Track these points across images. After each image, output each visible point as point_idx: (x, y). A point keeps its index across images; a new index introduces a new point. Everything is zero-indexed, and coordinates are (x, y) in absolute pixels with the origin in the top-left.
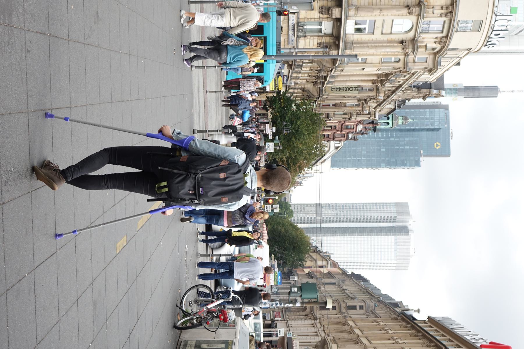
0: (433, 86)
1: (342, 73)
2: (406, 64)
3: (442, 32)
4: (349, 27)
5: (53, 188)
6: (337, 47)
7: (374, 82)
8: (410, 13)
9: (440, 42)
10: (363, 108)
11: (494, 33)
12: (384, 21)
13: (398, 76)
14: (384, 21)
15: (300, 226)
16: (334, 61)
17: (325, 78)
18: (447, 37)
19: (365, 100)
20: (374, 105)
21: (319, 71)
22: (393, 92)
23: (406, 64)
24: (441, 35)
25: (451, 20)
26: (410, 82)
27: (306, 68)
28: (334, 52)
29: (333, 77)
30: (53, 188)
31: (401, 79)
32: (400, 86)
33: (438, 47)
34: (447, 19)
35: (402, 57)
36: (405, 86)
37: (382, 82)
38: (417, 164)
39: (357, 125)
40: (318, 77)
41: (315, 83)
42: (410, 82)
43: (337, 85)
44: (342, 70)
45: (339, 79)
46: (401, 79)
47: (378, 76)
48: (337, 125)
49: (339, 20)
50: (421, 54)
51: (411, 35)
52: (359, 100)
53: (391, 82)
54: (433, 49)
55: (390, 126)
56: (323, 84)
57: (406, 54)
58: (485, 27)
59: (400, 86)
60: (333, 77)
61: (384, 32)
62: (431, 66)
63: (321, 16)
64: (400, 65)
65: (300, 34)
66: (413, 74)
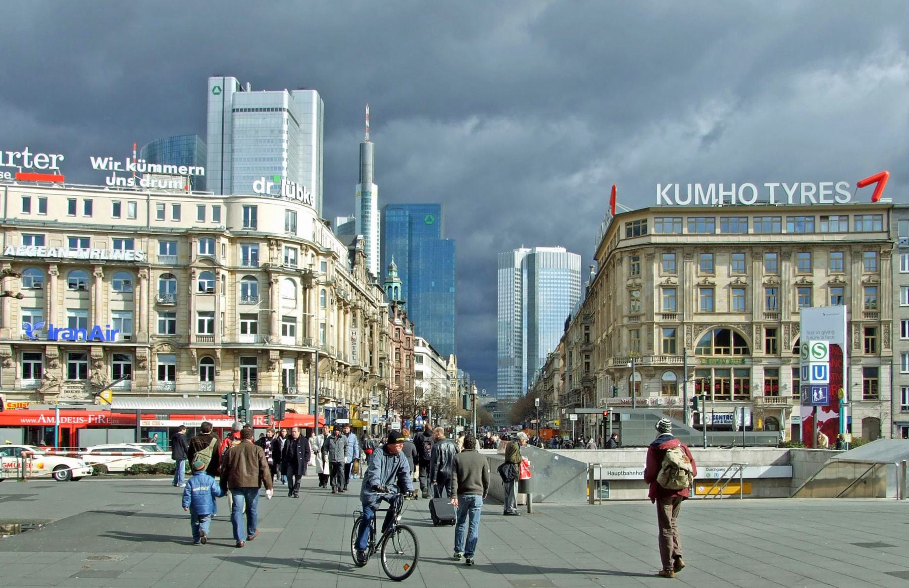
0: (352, 247)
1: (336, 347)
2: (328, 284)
3: (295, 249)
4: (289, 342)
5: (724, 288)
7: (346, 312)
8: (277, 281)
9: (306, 250)
10: (374, 321)
11: (298, 197)
12: (284, 307)
13: (340, 289)
14: (284, 307)
17: (340, 364)
18: (301, 244)
19: (366, 319)
20: (372, 308)
21: (333, 370)
22: (357, 290)
23: (328, 284)
24: (299, 251)
25: (285, 241)
26: (346, 274)
27: (330, 384)
28: (314, 356)
29: (339, 356)
30: (724, 288)
31: (343, 284)
32: (351, 284)
33: (311, 252)
34: (284, 245)
35: (321, 287)
36: (351, 278)
37: (345, 305)
39: (395, 325)
40: (339, 372)
41: (346, 374)
42: (346, 274)
43: (349, 352)
44: (332, 347)
45: (342, 349)
46: (343, 284)
47: (340, 308)
48: (394, 347)
49: (282, 352)
50: (317, 269)
52: (366, 326)
53: (346, 295)
54: (313, 256)
55: (399, 285)
56: (346, 366)
57: (317, 284)
58: (293, 206)
59: (351, 284)
60: (339, 356)
61: (236, 113)
62: (331, 258)
63: (277, 370)
65: (295, 391)
66: (338, 272)
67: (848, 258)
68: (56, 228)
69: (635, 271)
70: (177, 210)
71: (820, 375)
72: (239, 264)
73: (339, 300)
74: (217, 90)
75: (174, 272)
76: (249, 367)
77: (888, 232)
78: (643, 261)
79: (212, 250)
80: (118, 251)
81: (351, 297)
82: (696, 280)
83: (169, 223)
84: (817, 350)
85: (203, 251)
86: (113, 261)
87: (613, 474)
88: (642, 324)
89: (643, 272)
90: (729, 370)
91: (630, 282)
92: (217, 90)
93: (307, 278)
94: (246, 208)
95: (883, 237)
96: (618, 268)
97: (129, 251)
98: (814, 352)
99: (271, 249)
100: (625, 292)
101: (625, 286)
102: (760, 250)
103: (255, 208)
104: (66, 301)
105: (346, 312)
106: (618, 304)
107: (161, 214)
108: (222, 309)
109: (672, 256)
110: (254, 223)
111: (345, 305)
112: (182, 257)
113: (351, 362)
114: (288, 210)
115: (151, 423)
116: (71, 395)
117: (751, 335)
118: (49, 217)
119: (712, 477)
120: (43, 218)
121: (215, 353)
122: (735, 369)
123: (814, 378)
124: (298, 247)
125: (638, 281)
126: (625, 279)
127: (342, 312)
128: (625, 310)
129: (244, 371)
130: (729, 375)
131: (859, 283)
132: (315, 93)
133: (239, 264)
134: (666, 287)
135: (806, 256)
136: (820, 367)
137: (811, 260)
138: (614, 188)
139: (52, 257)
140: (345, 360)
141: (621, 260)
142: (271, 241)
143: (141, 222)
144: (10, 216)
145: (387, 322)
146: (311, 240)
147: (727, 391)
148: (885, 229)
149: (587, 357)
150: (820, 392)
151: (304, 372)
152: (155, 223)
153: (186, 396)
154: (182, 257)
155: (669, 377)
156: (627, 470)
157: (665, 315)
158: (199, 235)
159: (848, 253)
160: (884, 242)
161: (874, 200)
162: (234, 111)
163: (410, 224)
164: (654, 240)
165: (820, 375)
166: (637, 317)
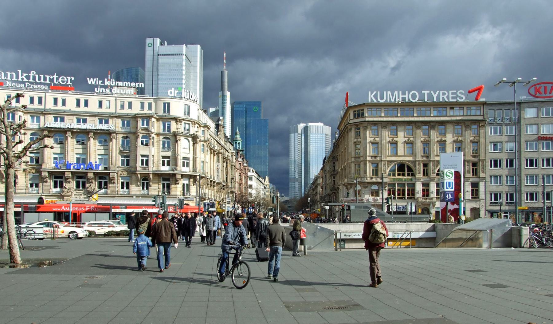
2: (205, 141)
3: (189, 124)
4: (186, 170)
6: (196, 176)
7: (214, 155)
8: (180, 140)
10: (228, 160)
13: (211, 144)
15: (303, 195)
16: (202, 177)
17: (211, 181)
18: (192, 122)
20: (227, 153)
21: (208, 184)
22: (220, 144)
23: (205, 141)
25: (184, 120)
26: (214, 136)
27: (207, 191)
28: (198, 177)
29: (211, 177)
31: (213, 141)
32: (217, 141)
33: (197, 125)
34: (183, 122)
35: (202, 143)
36: (217, 138)
37: (214, 151)
38: (266, 121)
40: (211, 185)
41: (214, 186)
42: (214, 136)
43: (215, 175)
45: (212, 174)
46: (213, 141)
47: (211, 153)
49: (182, 175)
50: (200, 134)
51: (190, 139)
53: (214, 147)
56: (214, 182)
58: (188, 103)
59: (217, 141)
60: (211, 177)
61: (159, 56)
62: (207, 128)
64: (205, 144)
67: (464, 129)
68: (70, 113)
69: (358, 135)
70: (130, 104)
71: (449, 187)
72: (161, 131)
73: (211, 149)
74: (150, 45)
75: (129, 135)
76: (166, 182)
77: (483, 115)
78: (362, 130)
79: (148, 124)
80: (101, 125)
81: (217, 148)
82: (388, 139)
83: (126, 111)
84: (451, 175)
85: (143, 125)
86: (98, 130)
87: (347, 236)
88: (361, 161)
89: (362, 135)
90: (404, 184)
91: (355, 140)
92: (150, 45)
93: (195, 138)
94: (165, 103)
95: (481, 118)
96: (349, 133)
97: (106, 125)
98: (447, 175)
99: (177, 124)
100: (353, 145)
101: (353, 142)
102: (420, 124)
103: (169, 104)
104: (75, 150)
105: (214, 155)
106: (349, 151)
107: (122, 107)
108: (153, 154)
109: (376, 127)
110: (169, 111)
111: (214, 151)
112: (133, 128)
113: (216, 180)
114: (185, 105)
115: (117, 211)
116: (78, 196)
117: (415, 166)
118: (67, 108)
119: (396, 237)
120: (64, 108)
121: (149, 176)
122: (408, 184)
123: (447, 188)
124: (191, 123)
125: (359, 140)
126: (353, 139)
127: (212, 155)
128: (353, 155)
129: (163, 185)
130: (405, 187)
131: (469, 141)
132: (199, 46)
133: (161, 131)
134: (373, 143)
135: (443, 127)
136: (449, 183)
137: (445, 129)
138: (347, 93)
139: (68, 128)
140: (214, 179)
141: (351, 129)
142: (177, 120)
143: (112, 110)
144: (47, 107)
145: (234, 160)
146: (197, 119)
147: (404, 194)
148: (482, 114)
149: (334, 178)
150: (450, 195)
151: (194, 185)
152: (119, 111)
153: (134, 197)
154: (133, 128)
155: (375, 187)
156: (354, 234)
157: (373, 157)
158: (141, 117)
159: (463, 126)
160: (482, 121)
161: (477, 99)
162: (158, 55)
163: (246, 111)
164: (367, 119)
165: (449, 187)
166: (359, 158)
